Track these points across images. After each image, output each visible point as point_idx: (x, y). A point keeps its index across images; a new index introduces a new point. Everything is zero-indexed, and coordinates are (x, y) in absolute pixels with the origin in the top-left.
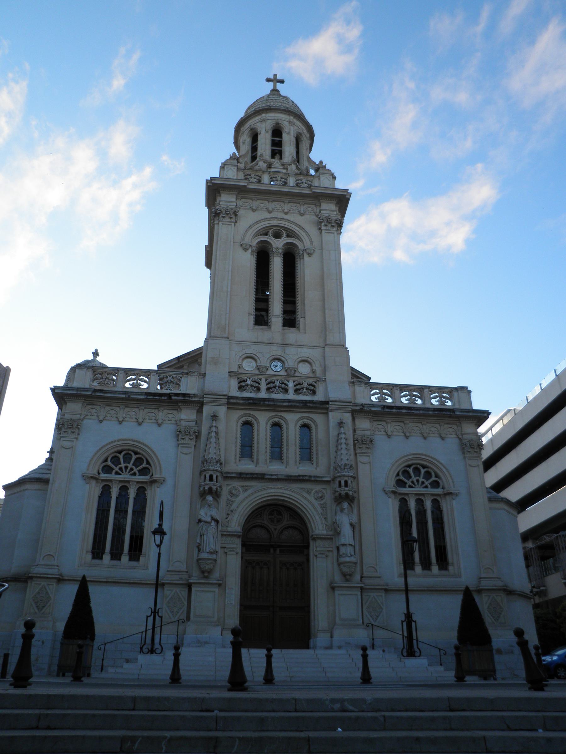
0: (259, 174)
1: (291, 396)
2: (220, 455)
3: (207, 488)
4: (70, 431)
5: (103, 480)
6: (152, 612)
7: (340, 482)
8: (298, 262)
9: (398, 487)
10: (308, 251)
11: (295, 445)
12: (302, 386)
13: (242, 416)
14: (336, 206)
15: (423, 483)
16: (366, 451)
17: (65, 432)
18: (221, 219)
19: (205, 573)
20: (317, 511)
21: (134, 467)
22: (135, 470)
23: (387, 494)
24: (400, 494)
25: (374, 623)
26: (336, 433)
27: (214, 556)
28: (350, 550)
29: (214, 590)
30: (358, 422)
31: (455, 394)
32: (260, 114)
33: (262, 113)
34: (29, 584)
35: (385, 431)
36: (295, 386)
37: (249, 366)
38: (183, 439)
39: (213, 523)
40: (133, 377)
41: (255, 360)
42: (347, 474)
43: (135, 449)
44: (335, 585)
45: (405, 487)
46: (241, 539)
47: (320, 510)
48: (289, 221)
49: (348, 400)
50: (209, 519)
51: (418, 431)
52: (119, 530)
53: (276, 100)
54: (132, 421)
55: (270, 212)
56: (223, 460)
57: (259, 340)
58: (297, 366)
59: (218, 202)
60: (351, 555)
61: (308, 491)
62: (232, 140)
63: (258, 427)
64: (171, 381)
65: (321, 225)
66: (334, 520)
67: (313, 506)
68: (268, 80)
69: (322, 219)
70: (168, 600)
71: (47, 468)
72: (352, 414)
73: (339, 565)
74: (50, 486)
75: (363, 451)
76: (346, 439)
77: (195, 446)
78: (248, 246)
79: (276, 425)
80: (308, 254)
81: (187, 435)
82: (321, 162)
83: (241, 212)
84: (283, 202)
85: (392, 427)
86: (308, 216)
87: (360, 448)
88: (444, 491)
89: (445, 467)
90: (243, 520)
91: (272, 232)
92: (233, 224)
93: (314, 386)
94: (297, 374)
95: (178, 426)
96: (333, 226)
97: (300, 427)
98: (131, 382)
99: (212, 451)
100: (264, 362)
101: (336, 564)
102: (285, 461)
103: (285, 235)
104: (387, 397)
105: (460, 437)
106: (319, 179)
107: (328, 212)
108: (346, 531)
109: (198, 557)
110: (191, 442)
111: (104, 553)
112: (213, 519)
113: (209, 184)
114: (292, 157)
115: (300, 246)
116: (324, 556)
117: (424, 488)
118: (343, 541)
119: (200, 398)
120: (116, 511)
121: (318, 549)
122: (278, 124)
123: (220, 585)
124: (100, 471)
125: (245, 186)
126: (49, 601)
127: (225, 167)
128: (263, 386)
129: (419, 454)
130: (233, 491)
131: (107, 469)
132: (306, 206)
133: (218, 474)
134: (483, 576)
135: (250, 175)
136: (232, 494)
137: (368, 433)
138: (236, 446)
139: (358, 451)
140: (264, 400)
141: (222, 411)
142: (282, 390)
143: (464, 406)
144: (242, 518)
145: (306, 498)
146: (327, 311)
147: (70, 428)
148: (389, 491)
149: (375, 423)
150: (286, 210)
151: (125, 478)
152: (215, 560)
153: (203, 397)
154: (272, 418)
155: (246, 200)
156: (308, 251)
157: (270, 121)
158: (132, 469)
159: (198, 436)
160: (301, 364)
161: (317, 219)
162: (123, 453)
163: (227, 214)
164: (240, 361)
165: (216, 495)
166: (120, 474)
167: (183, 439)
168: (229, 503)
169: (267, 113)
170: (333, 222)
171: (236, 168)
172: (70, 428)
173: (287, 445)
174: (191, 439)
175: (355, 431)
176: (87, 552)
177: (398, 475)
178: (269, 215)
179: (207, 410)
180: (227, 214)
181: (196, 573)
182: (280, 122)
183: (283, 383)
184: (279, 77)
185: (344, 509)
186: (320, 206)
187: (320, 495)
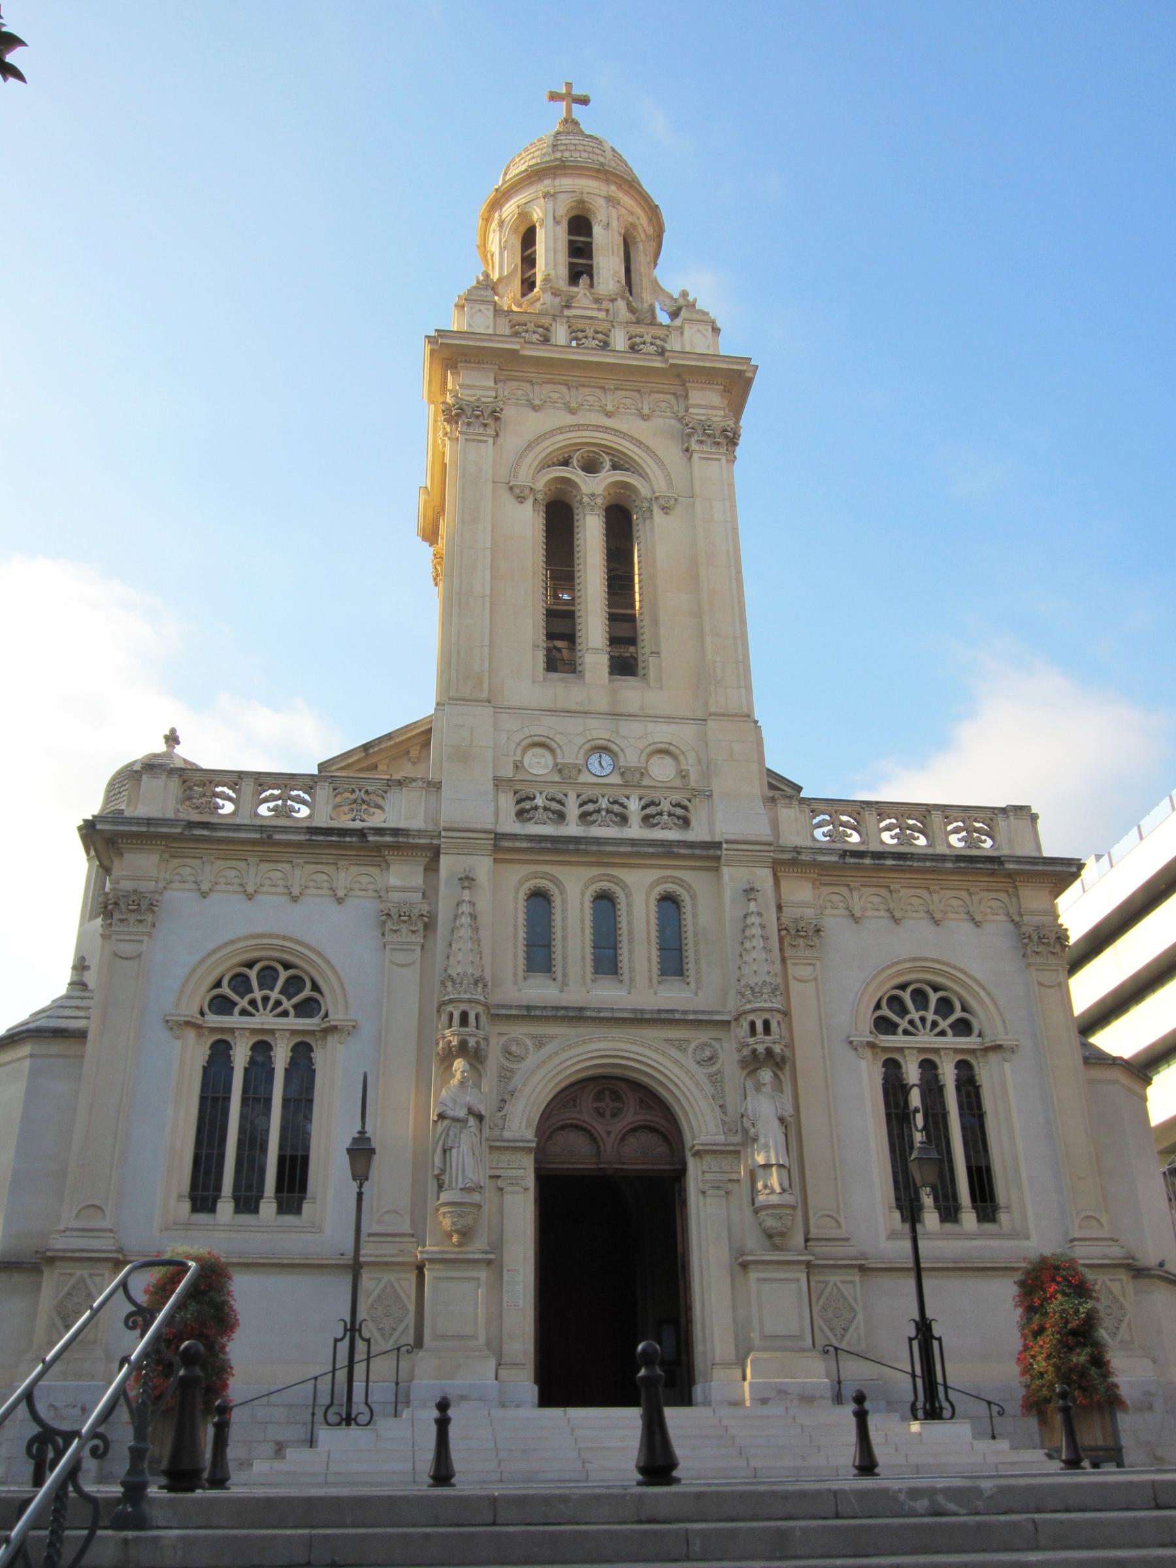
1: (635, 830)
4: (133, 917)
5: (213, 1030)
6: (346, 1330)
9: (880, 1033)
11: (649, 942)
17: (122, 920)
21: (284, 999)
22: (287, 1004)
25: (837, 1345)
29: (475, 1274)
30: (784, 885)
37: (539, 765)
39: (472, 1121)
40: (277, 792)
42: (769, 1005)
43: (285, 956)
48: (615, 432)
50: (462, 1113)
51: (921, 908)
52: (253, 1142)
57: (560, 706)
61: (680, 1045)
63: (564, 901)
64: (364, 801)
65: (688, 442)
67: (692, 1077)
68: (554, 97)
69: (693, 428)
75: (800, 953)
77: (423, 947)
81: (405, 922)
82: (684, 294)
83: (509, 413)
85: (865, 898)
86: (661, 421)
87: (794, 946)
88: (982, 1044)
92: (491, 440)
93: (685, 808)
98: (272, 805)
100: (570, 755)
103: (608, 465)
105: (1017, 919)
106: (682, 333)
116: (722, 1193)
122: (581, 203)
128: (573, 810)
131: (222, 1005)
137: (809, 912)
138: (515, 947)
139: (789, 953)
141: (482, 866)
142: (614, 818)
145: (676, 1061)
147: (133, 911)
148: (861, 1042)
151: (263, 1024)
156: (662, 502)
160: (655, 759)
163: (477, 417)
164: (519, 753)
166: (252, 1015)
168: (505, 1075)
170: (718, 433)
171: (492, 308)
172: (133, 911)
174: (414, 932)
177: (878, 1006)
178: (570, 420)
182: (586, 198)
183: (615, 802)
184: (576, 92)
186: (686, 397)
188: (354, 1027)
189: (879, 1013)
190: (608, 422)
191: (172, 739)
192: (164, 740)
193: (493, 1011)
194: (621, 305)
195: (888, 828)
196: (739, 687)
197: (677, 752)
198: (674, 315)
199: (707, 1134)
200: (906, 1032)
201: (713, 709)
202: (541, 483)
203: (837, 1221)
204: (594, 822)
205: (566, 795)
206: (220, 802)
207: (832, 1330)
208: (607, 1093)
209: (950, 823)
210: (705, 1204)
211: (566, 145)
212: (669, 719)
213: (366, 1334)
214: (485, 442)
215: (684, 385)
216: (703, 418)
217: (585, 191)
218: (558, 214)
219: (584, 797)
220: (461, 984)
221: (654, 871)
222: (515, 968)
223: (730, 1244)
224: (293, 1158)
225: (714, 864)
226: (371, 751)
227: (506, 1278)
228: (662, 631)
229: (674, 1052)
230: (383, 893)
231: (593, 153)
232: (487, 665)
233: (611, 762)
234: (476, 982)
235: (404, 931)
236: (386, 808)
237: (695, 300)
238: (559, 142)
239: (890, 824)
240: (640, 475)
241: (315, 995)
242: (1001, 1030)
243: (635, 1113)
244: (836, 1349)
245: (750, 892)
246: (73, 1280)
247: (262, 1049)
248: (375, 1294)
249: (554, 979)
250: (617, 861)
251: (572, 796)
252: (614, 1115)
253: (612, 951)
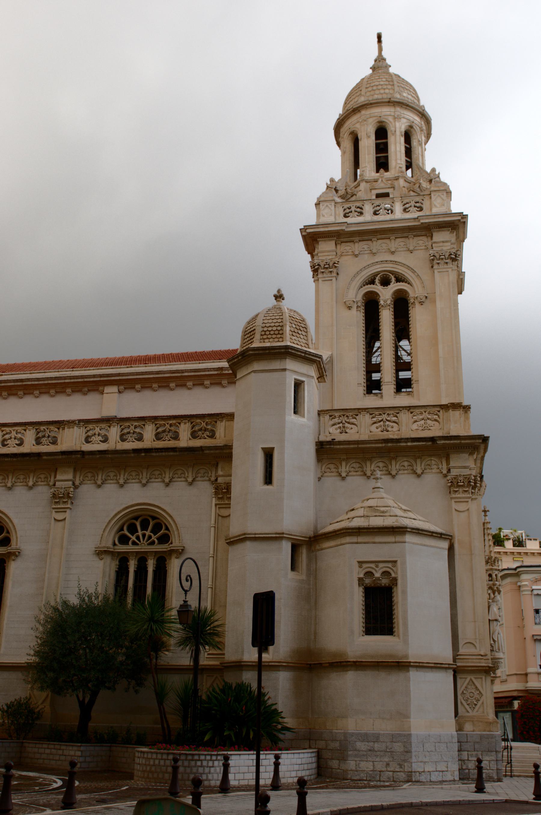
16: (464, 496)
22: (154, 538)
48: (395, 262)
91: (379, 279)
92: (334, 279)
103: (393, 279)
106: (431, 198)
115: (412, 294)
124: (117, 542)
131: (124, 540)
135: (349, 208)
166: (137, 544)
171: (333, 203)
188: (182, 550)
192: (274, 298)
202: (360, 297)
237: (439, 173)
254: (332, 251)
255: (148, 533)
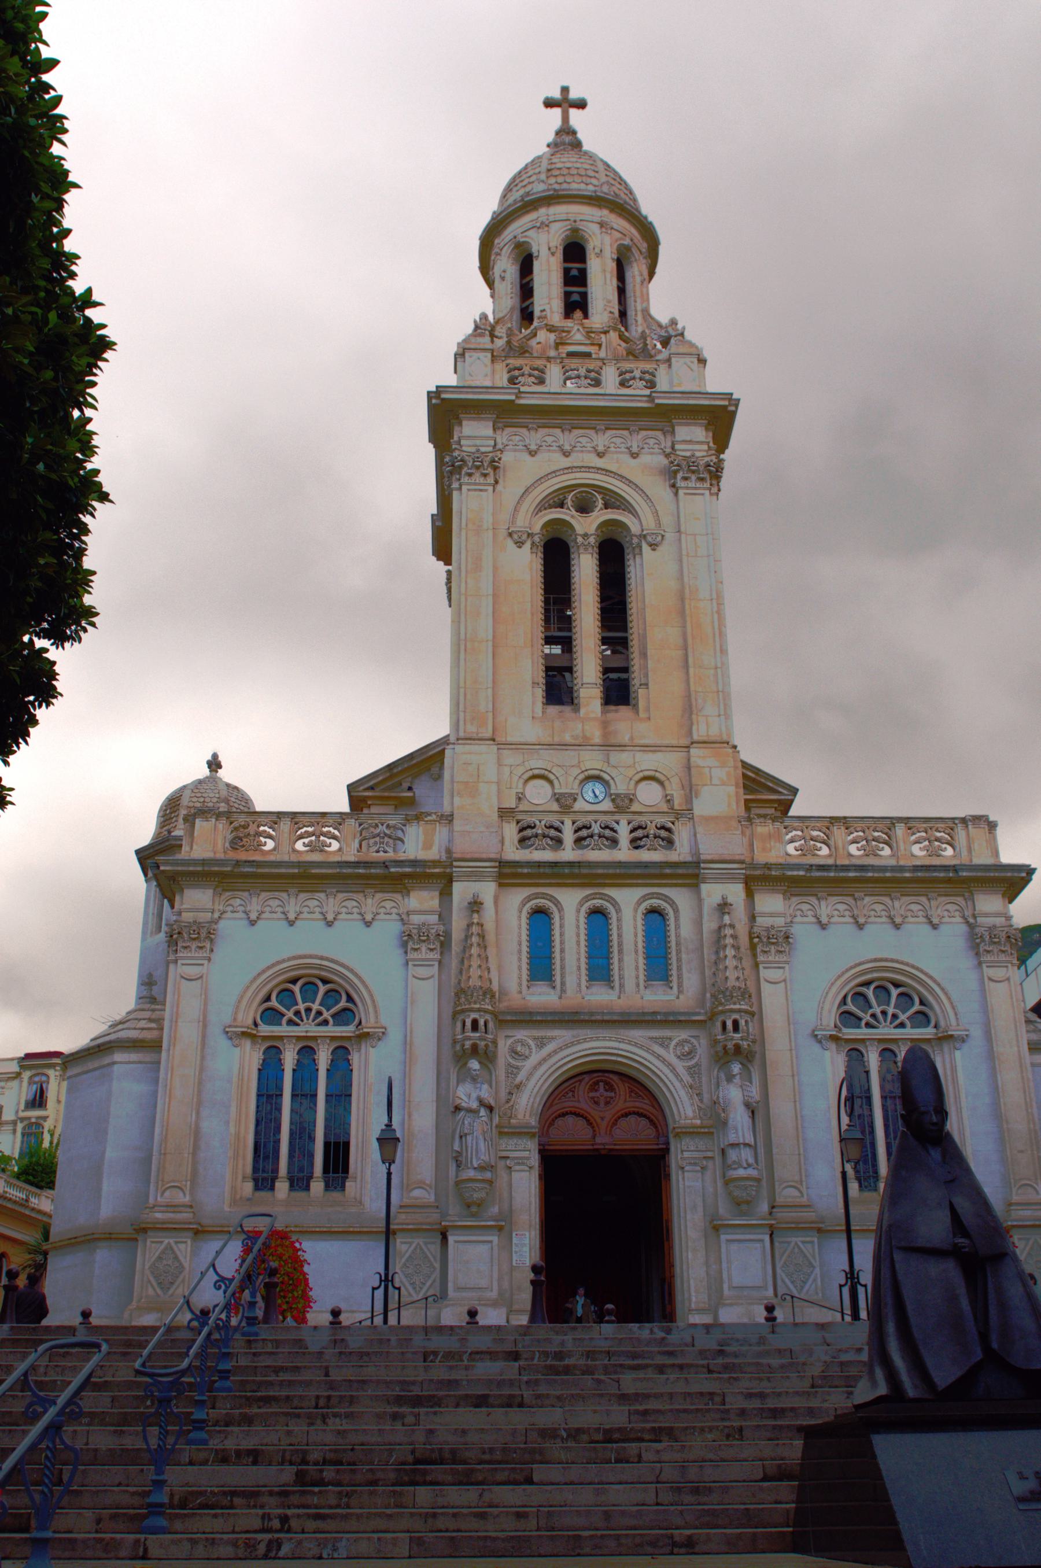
0: (539, 363)
1: (624, 853)
2: (490, 981)
3: (468, 1044)
4: (194, 945)
5: (265, 1038)
6: (381, 1281)
7: (724, 1024)
8: (631, 562)
9: (845, 1026)
10: (649, 539)
11: (636, 952)
12: (645, 832)
13: (529, 899)
14: (707, 429)
15: (895, 1016)
17: (186, 948)
18: (465, 479)
19: (472, 1207)
20: (681, 1081)
21: (323, 1010)
23: (820, 1042)
24: (848, 1041)
25: (795, 1293)
26: (714, 925)
27: (488, 1175)
28: (747, 1155)
29: (490, 1238)
30: (758, 898)
31: (961, 833)
32: (536, 209)
33: (541, 206)
34: (140, 1244)
35: (815, 916)
36: (632, 832)
37: (539, 794)
38: (416, 950)
39: (483, 1112)
40: (310, 829)
41: (551, 782)
42: (737, 1007)
43: (323, 973)
44: (720, 1222)
45: (859, 1027)
46: (537, 1140)
47: (687, 1078)
48: (607, 472)
49: (737, 858)
50: (474, 1105)
51: (884, 913)
52: (302, 1133)
53: (569, 168)
54: (313, 919)
55: (566, 454)
56: (495, 986)
57: (557, 740)
58: (635, 789)
59: (456, 438)
60: (749, 1165)
61: (663, 1042)
62: (476, 262)
63: (562, 918)
64: (386, 835)
65: (675, 478)
66: (715, 1098)
67: (673, 1070)
68: (549, 104)
69: (678, 465)
70: (403, 1260)
71: (147, 1017)
72: (746, 884)
73: (727, 1183)
74: (164, 1054)
75: (770, 958)
76: (734, 937)
77: (440, 962)
78: (524, 537)
79: (597, 912)
80: (651, 545)
81: (424, 941)
82: (673, 322)
83: (507, 458)
84: (595, 428)
85: (829, 907)
86: (649, 457)
87: (765, 952)
88: (936, 1034)
89: (939, 985)
90: (538, 1103)
92: (491, 488)
93: (669, 830)
94: (635, 807)
95: (404, 924)
96: (702, 479)
97: (645, 915)
98: (306, 841)
99: (475, 972)
100: (567, 784)
101: (720, 1184)
102: (617, 984)
103: (600, 503)
104: (819, 845)
105: (971, 920)
106: (670, 366)
107: (690, 447)
108: (739, 1117)
109: (457, 1177)
110: (431, 955)
111: (276, 1177)
112: (482, 1103)
113: (434, 401)
114: (611, 312)
115: (634, 528)
116: (698, 1168)
117: (896, 1027)
118: (732, 1138)
119: (445, 867)
120: (294, 1096)
121: (686, 1154)
122: (575, 231)
123: (500, 1229)
125: (512, 401)
126: (180, 1273)
127: (467, 355)
128: (568, 836)
129: (886, 960)
130: (519, 1049)
131: (271, 1015)
132: (644, 433)
133: (488, 1017)
134: (1015, 1198)
135: (520, 369)
136: (516, 1053)
137: (780, 922)
138: (520, 960)
139: (761, 958)
140: (571, 864)
141: (487, 890)
142: (606, 842)
143: (982, 858)
144: (538, 1099)
145: (659, 1057)
146: (691, 670)
147: (194, 939)
148: (824, 1035)
149: (794, 899)
150: (601, 448)
151: (307, 1032)
152: (490, 1182)
153: (451, 866)
154: (587, 899)
155: (515, 429)
156: (649, 539)
157: (557, 225)
158: (319, 1013)
159: (444, 943)
160: (643, 785)
161: (665, 461)
162: (300, 983)
163: (478, 468)
164: (520, 785)
165: (486, 1056)
166: (298, 1025)
167: (416, 950)
168: (512, 1071)
169: (549, 205)
170: (701, 468)
171: (489, 355)
172: (194, 939)
173: (620, 952)
174: (432, 950)
175: (753, 918)
176: (244, 1178)
177: (844, 1001)
178: (566, 462)
179: (461, 891)
180: (478, 468)
181: (454, 1209)
182: (581, 226)
183: (607, 827)
184: (573, 95)
185: (734, 1076)
186: (673, 433)
187: (686, 1049)
188: (383, 1033)
189: (844, 1008)
190: (600, 463)
191: (214, 764)
193: (501, 1018)
194: (613, 335)
195: (854, 841)
196: (719, 716)
197: (662, 778)
198: (665, 343)
199: (686, 1118)
200: (868, 1025)
201: (696, 737)
202: (537, 528)
203: (801, 1192)
204: (588, 846)
205: (563, 823)
206: (263, 839)
207: (792, 1282)
208: (601, 1084)
209: (914, 834)
210: (683, 1178)
211: (560, 169)
212: (654, 748)
213: (397, 1285)
214: (486, 490)
215: (670, 422)
216: (688, 454)
217: (578, 219)
218: (553, 244)
219: (579, 824)
220: (472, 995)
221: (640, 889)
222: (520, 978)
223: (704, 1210)
224: (337, 1144)
225: (695, 881)
226: (395, 771)
227: (515, 1240)
228: (651, 664)
229: (657, 1048)
230: (404, 916)
231: (587, 176)
232: (491, 706)
233: (603, 790)
234: (485, 994)
235: (424, 949)
236: (406, 840)
237: (684, 328)
238: (553, 166)
239: (857, 836)
240: (630, 512)
241: (350, 1005)
242: (953, 1022)
243: (625, 1101)
244: (792, 1297)
245: (724, 907)
246: (163, 1247)
247: (307, 1051)
248: (407, 1255)
249: (554, 988)
250: (607, 881)
251: (568, 823)
252: (607, 1103)
253: (605, 961)
254: (488, 438)
255: (903, 1017)
